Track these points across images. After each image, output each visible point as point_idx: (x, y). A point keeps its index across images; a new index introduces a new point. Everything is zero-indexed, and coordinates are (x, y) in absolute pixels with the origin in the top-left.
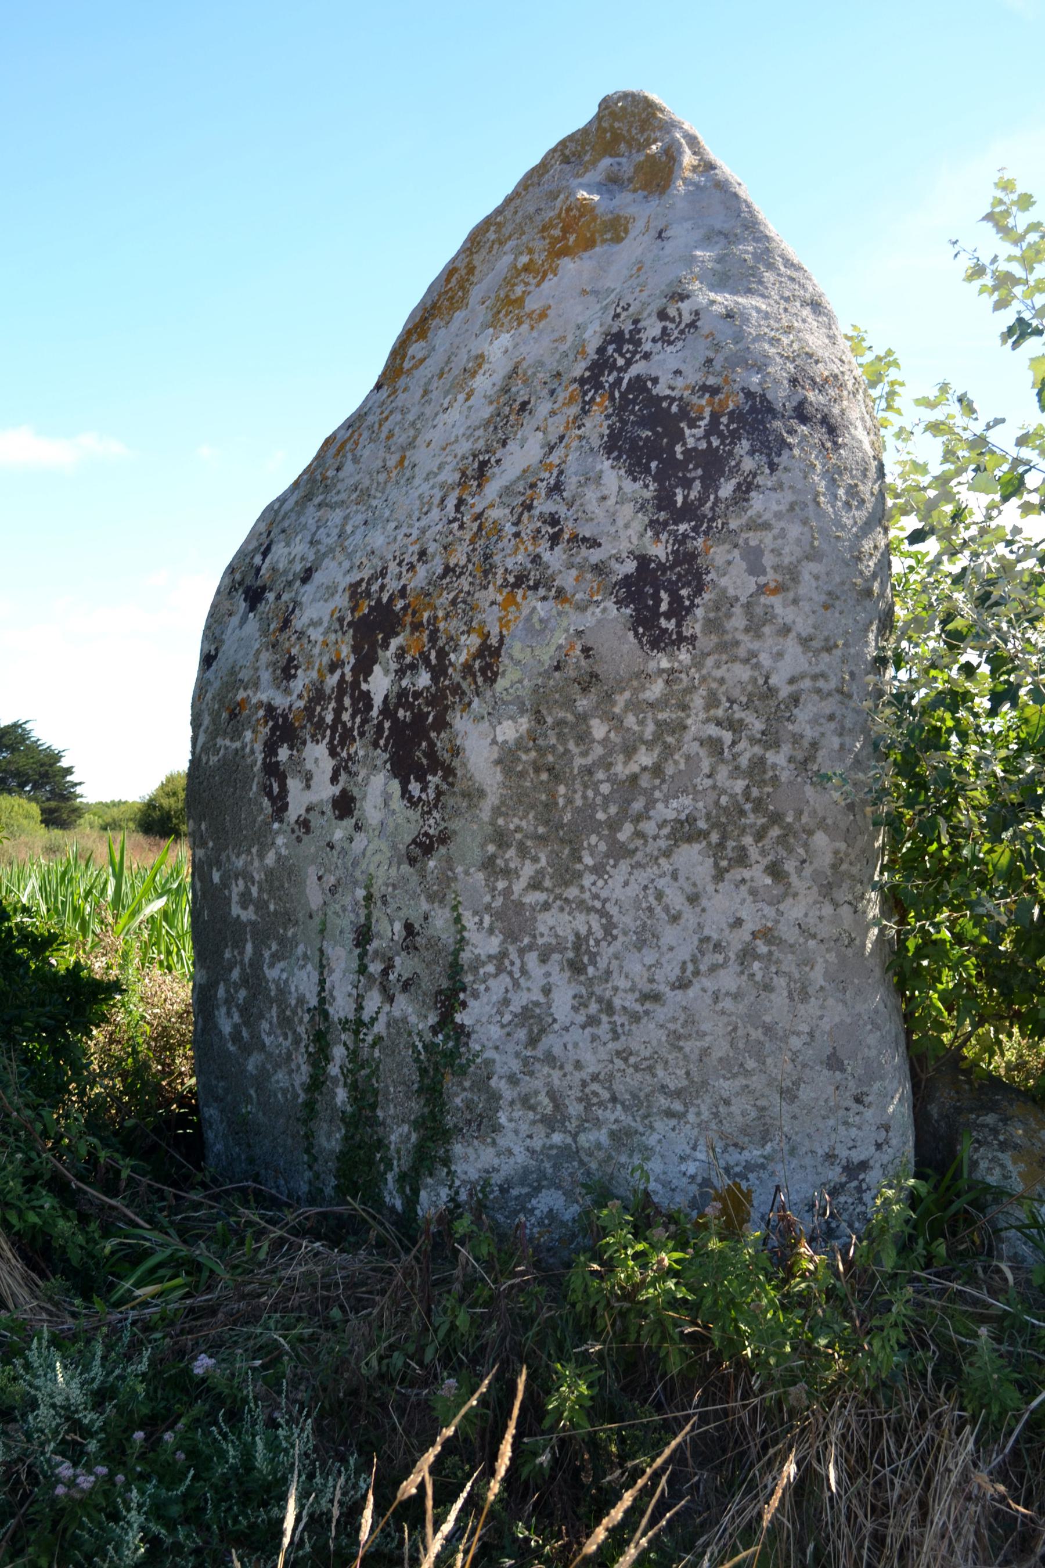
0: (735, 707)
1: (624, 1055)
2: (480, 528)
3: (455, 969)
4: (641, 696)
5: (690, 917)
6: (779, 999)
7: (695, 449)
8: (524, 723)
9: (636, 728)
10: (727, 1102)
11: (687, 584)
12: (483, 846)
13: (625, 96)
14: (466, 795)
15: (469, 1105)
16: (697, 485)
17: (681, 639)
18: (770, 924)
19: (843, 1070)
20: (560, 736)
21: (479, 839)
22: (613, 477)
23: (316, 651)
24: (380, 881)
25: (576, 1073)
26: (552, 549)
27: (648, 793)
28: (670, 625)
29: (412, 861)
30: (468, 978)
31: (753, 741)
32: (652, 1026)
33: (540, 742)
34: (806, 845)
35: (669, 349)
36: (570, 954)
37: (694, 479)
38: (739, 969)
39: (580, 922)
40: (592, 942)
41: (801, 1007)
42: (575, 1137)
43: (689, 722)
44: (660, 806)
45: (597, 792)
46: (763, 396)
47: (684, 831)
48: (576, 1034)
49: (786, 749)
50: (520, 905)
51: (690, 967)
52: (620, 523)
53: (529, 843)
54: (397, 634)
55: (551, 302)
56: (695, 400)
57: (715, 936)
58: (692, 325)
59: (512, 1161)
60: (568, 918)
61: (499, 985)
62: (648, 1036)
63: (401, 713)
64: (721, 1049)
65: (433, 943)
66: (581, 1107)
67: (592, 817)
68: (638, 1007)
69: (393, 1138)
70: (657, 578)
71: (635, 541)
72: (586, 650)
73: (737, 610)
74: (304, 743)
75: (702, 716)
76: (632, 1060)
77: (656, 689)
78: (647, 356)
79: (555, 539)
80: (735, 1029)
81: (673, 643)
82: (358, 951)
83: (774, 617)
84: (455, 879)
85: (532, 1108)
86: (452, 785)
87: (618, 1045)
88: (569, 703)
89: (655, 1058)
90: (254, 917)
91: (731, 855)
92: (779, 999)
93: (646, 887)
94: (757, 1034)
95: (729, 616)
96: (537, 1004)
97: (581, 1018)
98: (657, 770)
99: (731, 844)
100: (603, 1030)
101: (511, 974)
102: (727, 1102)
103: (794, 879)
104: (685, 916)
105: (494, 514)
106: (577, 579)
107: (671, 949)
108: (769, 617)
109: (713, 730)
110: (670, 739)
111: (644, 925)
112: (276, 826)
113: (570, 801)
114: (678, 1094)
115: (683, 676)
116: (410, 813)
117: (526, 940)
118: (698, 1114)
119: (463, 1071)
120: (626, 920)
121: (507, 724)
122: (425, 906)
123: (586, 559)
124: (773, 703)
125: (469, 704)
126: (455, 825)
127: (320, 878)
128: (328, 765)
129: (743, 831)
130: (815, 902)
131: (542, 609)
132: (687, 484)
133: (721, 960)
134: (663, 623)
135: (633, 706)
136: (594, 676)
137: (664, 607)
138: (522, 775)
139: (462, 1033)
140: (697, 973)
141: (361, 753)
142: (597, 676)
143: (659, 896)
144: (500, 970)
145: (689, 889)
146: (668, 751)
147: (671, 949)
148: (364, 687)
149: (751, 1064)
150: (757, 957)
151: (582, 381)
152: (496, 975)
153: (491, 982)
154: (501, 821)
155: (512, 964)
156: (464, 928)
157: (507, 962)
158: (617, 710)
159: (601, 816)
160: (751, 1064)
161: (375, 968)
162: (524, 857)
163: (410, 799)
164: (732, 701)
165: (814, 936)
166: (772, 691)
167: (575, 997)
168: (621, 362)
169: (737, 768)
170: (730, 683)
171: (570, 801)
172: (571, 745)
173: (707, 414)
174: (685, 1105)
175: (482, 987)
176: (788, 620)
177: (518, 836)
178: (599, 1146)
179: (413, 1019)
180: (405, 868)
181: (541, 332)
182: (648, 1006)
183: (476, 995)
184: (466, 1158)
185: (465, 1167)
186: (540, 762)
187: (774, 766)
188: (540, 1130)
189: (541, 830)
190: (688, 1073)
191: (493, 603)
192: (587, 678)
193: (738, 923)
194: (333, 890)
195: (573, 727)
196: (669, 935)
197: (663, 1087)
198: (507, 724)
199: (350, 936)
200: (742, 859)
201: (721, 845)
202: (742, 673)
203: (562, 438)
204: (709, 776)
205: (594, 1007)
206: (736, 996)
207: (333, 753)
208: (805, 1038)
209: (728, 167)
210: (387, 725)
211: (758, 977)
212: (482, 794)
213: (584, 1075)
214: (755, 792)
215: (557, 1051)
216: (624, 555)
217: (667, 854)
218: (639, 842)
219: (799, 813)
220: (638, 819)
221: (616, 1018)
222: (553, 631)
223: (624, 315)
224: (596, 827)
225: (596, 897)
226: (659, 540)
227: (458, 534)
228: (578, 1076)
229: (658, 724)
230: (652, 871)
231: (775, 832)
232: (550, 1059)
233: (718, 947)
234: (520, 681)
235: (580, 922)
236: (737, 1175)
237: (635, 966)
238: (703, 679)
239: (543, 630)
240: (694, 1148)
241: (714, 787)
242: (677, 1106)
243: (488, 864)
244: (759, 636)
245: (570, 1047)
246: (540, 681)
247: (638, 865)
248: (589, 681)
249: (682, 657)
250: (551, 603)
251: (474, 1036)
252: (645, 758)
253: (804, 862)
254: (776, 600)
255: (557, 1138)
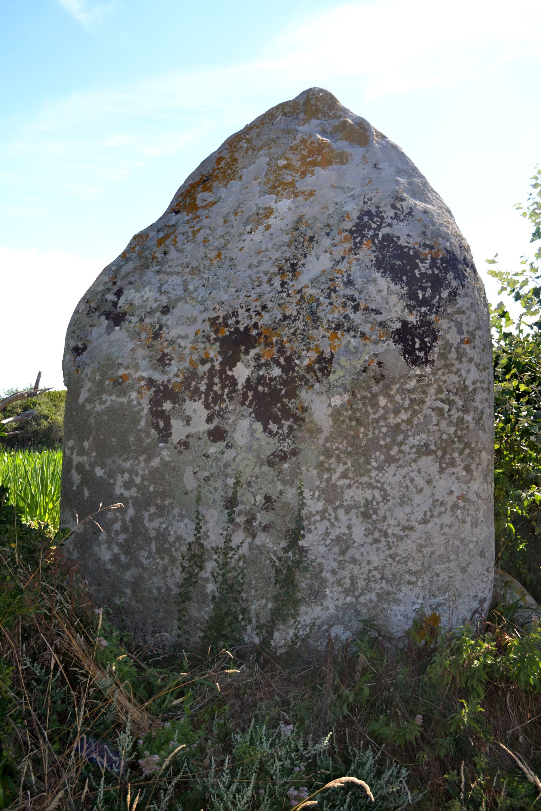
0: (451, 394)
1: (393, 557)
2: (302, 297)
3: (299, 519)
4: (405, 387)
5: (427, 490)
6: (468, 526)
7: (426, 273)
8: (346, 397)
9: (401, 401)
10: (438, 575)
11: (428, 336)
12: (317, 457)
13: (321, 90)
14: (309, 431)
15: (310, 587)
16: (429, 290)
17: (427, 361)
18: (464, 493)
19: (485, 557)
20: (364, 404)
21: (315, 454)
22: (384, 282)
23: (187, 351)
24: (247, 475)
25: (367, 567)
26: (355, 313)
27: (405, 433)
28: (422, 354)
29: (271, 464)
30: (305, 523)
31: (458, 410)
32: (409, 542)
33: (354, 406)
34: (479, 458)
35: (402, 224)
36: (363, 509)
37: (427, 287)
38: (452, 514)
39: (368, 494)
40: (375, 503)
41: (475, 530)
42: (357, 598)
43: (427, 400)
44: (411, 438)
45: (380, 431)
46: (453, 252)
47: (424, 450)
48: (367, 548)
49: (472, 413)
50: (335, 486)
51: (429, 514)
52: (391, 304)
53: (342, 455)
54: (255, 347)
55: (315, 188)
56: (421, 250)
57: (441, 499)
58: (409, 213)
59: (327, 613)
60: (361, 492)
61: (322, 526)
62: (408, 546)
63: (260, 388)
64: (441, 551)
65: (285, 506)
66: (364, 583)
67: (377, 443)
68: (402, 534)
69: (253, 607)
70: (412, 332)
71: (400, 313)
72: (379, 364)
73: (453, 350)
74: (184, 401)
75: (434, 397)
76: (397, 559)
77: (412, 384)
78: (390, 225)
79: (356, 308)
80: (448, 542)
81: (423, 363)
82: (226, 511)
83: (467, 354)
84: (301, 473)
85: (341, 586)
86: (300, 426)
87: (391, 552)
88: (369, 387)
89: (410, 557)
90: (135, 494)
91: (448, 461)
92: (468, 526)
93: (405, 477)
94: (457, 543)
95: (450, 352)
96: (344, 534)
97: (370, 540)
98: (409, 422)
99: (448, 456)
100: (383, 545)
101: (329, 520)
102: (438, 575)
103: (475, 473)
104: (425, 490)
105: (310, 291)
106: (371, 329)
107: (418, 505)
108: (465, 354)
109: (439, 404)
110: (416, 407)
111: (404, 494)
112: (161, 445)
113: (366, 435)
114: (415, 573)
115: (426, 378)
116: (271, 440)
117: (338, 503)
118: (423, 582)
119: (306, 569)
120: (395, 492)
121: (337, 397)
122: (280, 487)
123: (375, 320)
124: (467, 393)
125: (312, 386)
126: (302, 446)
127: (195, 473)
128: (204, 413)
129: (453, 450)
130: (482, 483)
131: (354, 342)
132: (424, 289)
133: (443, 510)
134: (417, 353)
135: (402, 391)
136: (383, 376)
137: (417, 346)
138: (343, 421)
139: (303, 551)
140: (432, 516)
141: (231, 408)
142: (384, 376)
143: (412, 480)
144: (323, 518)
145: (427, 478)
146: (415, 413)
147: (418, 505)
148: (229, 373)
149: (453, 557)
150: (459, 508)
151: (351, 232)
152: (321, 521)
153: (318, 525)
154: (328, 445)
155: (330, 515)
156: (304, 498)
157: (327, 514)
158: (392, 393)
159: (382, 443)
160: (453, 557)
161: (241, 520)
162: (339, 462)
163: (271, 432)
164: (449, 391)
165: (481, 498)
166: (466, 387)
167: (366, 530)
168: (374, 226)
169: (451, 422)
170: (449, 383)
171: (366, 435)
172: (369, 408)
173: (429, 256)
174: (417, 578)
175: (313, 527)
176: (472, 355)
177: (337, 452)
178: (371, 601)
179: (270, 545)
180: (265, 468)
181: (312, 202)
182: (407, 532)
183: (310, 531)
184: (306, 613)
185: (305, 618)
186: (353, 417)
187: (467, 422)
188: (343, 595)
189: (349, 449)
190: (423, 563)
191: (323, 337)
192: (379, 377)
193: (451, 492)
194: (207, 479)
195: (370, 400)
196: (417, 499)
197: (410, 570)
198: (337, 397)
199: (221, 504)
200: (452, 463)
201: (443, 457)
202: (454, 378)
203: (343, 258)
204: (436, 425)
205: (377, 535)
206: (450, 526)
207: (207, 406)
208: (474, 544)
209: (393, 138)
210: (250, 394)
211: (460, 517)
212: (320, 431)
213: (371, 567)
214: (459, 433)
215: (358, 556)
216: (395, 319)
217: (415, 461)
218: (401, 455)
219: (477, 442)
220: (400, 444)
221: (389, 539)
222: (361, 353)
223: (369, 203)
224: (380, 448)
225: (378, 481)
226: (412, 314)
227: (288, 299)
228: (368, 568)
229: (411, 400)
230: (407, 469)
231: (467, 451)
232: (354, 561)
233: (442, 504)
234: (344, 376)
235: (368, 494)
236: (434, 609)
237: (400, 514)
238: (436, 380)
239: (357, 352)
240: (417, 599)
241: (439, 430)
242: (413, 579)
243: (320, 466)
244: (461, 362)
245: (365, 554)
246: (355, 377)
247: (401, 466)
248: (379, 378)
249: (427, 370)
250: (358, 340)
251: (310, 552)
252: (404, 416)
253: (478, 464)
254: (467, 346)
255: (348, 599)
